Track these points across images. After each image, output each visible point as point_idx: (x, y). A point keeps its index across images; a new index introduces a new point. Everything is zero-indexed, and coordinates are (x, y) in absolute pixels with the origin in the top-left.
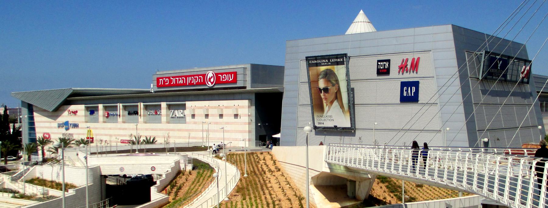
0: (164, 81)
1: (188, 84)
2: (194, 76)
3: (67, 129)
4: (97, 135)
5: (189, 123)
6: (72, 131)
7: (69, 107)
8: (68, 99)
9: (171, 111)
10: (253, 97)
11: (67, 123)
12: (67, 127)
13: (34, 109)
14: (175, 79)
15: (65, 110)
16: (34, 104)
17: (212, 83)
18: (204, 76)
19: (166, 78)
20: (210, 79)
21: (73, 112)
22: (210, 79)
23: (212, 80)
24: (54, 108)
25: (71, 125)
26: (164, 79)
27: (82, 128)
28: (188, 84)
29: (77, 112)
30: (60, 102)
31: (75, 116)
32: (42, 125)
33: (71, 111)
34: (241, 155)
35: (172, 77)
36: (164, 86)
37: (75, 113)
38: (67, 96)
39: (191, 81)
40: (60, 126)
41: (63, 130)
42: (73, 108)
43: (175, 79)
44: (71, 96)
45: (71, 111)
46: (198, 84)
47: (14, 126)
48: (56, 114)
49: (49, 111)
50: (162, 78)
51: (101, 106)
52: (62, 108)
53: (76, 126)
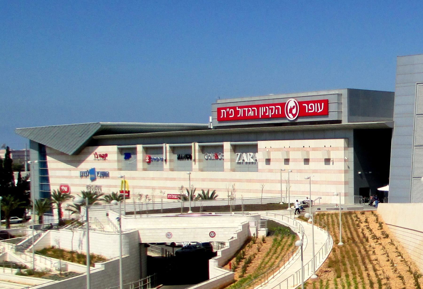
0: (228, 113)
1: (260, 117)
2: (268, 105)
3: (93, 179)
4: (134, 187)
5: (263, 171)
6: (99, 181)
7: (95, 149)
8: (95, 137)
9: (238, 154)
10: (351, 135)
11: (92, 171)
12: (93, 176)
13: (48, 151)
14: (242, 109)
15: (90, 153)
16: (48, 145)
17: (294, 115)
18: (283, 105)
19: (230, 108)
20: (291, 110)
21: (101, 156)
22: (291, 110)
23: (294, 111)
24: (75, 150)
25: (98, 173)
26: (228, 110)
27: (114, 178)
28: (260, 117)
29: (106, 155)
30: (83, 142)
31: (104, 161)
32: (58, 173)
33: (98, 154)
34: (334, 216)
35: (239, 107)
36: (227, 119)
37: (104, 156)
38: (93, 133)
39: (265, 113)
40: (83, 175)
41: (87, 181)
42: (101, 149)
43: (242, 109)
44: (98, 133)
45: (98, 154)
46: (274, 117)
47: (19, 175)
48: (77, 158)
49: (68, 155)
50: (225, 108)
51: (140, 148)
52: (85, 150)
53: (105, 175)
